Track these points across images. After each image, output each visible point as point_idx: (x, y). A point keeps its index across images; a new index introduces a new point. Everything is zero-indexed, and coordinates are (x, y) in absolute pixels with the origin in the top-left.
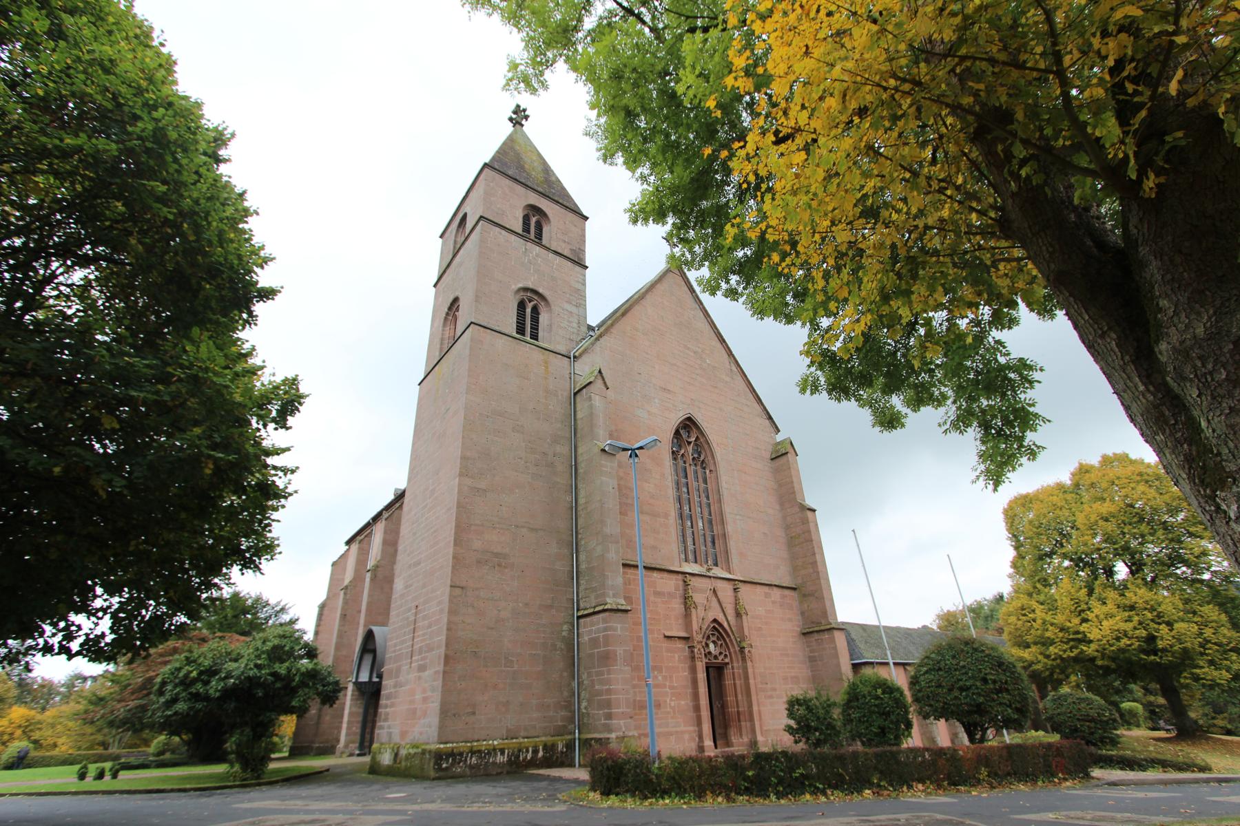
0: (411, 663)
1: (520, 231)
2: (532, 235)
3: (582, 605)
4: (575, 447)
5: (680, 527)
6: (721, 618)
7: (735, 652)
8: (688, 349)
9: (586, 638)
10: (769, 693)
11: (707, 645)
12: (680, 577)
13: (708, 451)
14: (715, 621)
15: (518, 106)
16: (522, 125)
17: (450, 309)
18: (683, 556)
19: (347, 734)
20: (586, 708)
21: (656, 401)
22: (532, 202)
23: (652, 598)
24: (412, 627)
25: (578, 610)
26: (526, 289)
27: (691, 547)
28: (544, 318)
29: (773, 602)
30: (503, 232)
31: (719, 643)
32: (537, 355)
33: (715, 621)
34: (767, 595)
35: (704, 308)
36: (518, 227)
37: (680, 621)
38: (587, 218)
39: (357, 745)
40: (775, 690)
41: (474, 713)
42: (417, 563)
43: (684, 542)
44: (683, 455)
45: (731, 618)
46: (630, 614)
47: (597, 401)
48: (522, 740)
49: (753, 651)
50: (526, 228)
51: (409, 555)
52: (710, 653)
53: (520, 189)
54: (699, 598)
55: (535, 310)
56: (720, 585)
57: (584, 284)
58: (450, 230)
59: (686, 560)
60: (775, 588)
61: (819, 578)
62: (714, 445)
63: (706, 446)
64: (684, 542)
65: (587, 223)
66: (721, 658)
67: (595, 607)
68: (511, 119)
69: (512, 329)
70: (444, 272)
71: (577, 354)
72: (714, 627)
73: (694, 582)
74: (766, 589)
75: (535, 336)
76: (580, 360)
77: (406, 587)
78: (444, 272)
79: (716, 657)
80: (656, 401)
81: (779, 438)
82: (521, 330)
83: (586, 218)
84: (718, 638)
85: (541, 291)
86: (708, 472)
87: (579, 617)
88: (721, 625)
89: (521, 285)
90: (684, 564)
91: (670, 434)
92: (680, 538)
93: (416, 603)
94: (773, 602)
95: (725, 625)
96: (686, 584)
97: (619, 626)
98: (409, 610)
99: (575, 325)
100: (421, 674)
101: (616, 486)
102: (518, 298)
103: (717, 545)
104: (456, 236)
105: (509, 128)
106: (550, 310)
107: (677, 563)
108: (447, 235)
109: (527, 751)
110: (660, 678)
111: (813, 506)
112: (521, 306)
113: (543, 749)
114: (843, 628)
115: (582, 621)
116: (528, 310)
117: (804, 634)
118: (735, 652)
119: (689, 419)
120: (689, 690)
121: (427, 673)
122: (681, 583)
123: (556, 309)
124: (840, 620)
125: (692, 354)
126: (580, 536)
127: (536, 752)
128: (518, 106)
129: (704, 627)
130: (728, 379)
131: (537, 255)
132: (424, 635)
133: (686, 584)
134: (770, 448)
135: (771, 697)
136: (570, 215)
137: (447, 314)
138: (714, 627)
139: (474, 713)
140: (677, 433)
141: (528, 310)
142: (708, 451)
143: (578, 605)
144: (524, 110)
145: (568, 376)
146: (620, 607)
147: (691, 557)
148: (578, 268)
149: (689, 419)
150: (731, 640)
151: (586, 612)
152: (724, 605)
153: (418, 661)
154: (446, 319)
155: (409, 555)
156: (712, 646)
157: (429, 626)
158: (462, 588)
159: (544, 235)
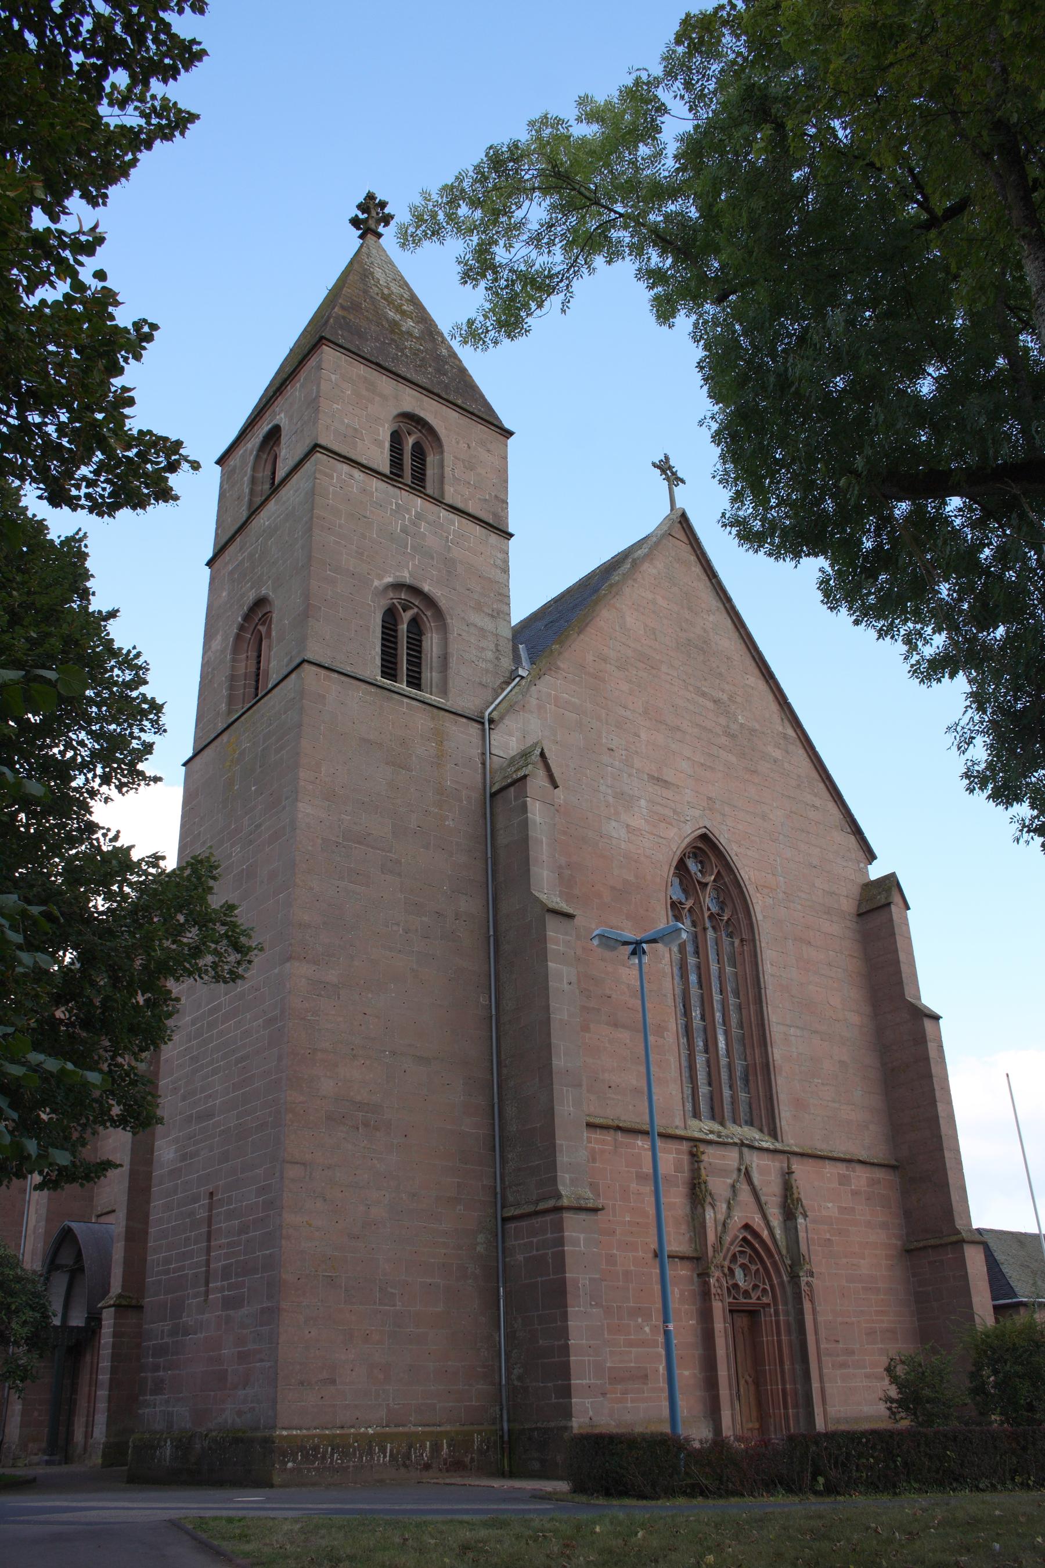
0: (207, 1293)
1: (387, 471)
2: (408, 478)
3: (511, 1199)
4: (495, 900)
5: (684, 1052)
6: (757, 1222)
7: (782, 1284)
8: (704, 695)
9: (520, 1258)
10: (841, 1359)
11: (731, 1271)
12: (685, 1146)
13: (738, 902)
14: (747, 1227)
15: (370, 197)
16: (379, 235)
17: (247, 618)
18: (689, 1106)
19: (23, 1425)
20: (520, 1378)
21: (643, 803)
22: (407, 408)
23: (634, 1186)
24: (205, 1230)
25: (503, 1207)
26: (398, 586)
27: (703, 1090)
28: (431, 643)
29: (855, 1193)
30: (357, 473)
31: (753, 1268)
32: (421, 721)
33: (747, 1227)
34: (844, 1180)
35: (733, 608)
36: (382, 460)
37: (684, 1228)
38: (509, 434)
39: (44, 1445)
40: (851, 1352)
41: (333, 1382)
42: (208, 1115)
43: (693, 1079)
44: (691, 910)
45: (776, 1222)
46: (600, 1216)
47: (537, 813)
48: (413, 1429)
49: (815, 1281)
50: (396, 461)
51: (184, 1099)
52: (736, 1286)
53: (385, 384)
54: (718, 1186)
55: (416, 627)
56: (755, 1161)
57: (506, 570)
58: (240, 451)
59: (696, 1114)
60: (859, 1168)
61: (941, 1149)
62: (751, 889)
63: (734, 892)
64: (693, 1079)
65: (511, 441)
66: (754, 1295)
67: (537, 1202)
68: (355, 222)
69: (373, 670)
70: (232, 539)
71: (495, 715)
72: (744, 1239)
73: (711, 1156)
74: (841, 1168)
75: (415, 681)
76: (501, 727)
77: (184, 1158)
78: (232, 539)
79: (746, 1294)
80: (643, 803)
81: (876, 871)
82: (389, 669)
83: (509, 434)
84: (751, 1260)
85: (426, 588)
86: (737, 942)
87: (505, 1220)
88: (756, 1235)
89: (389, 580)
90: (694, 1123)
91: (666, 870)
92: (686, 1074)
93: (210, 1188)
94: (855, 1193)
95: (765, 1234)
96: (695, 1157)
97: (582, 1236)
98: (195, 1199)
99: (489, 655)
100: (231, 1312)
101: (574, 979)
102: (384, 603)
103: (752, 1084)
104: (254, 469)
105: (352, 238)
106: (444, 628)
107: (678, 1121)
108: (233, 461)
109: (423, 1446)
110: (647, 1329)
111: (936, 1009)
112: (390, 618)
113: (449, 1446)
114: (984, 1239)
115: (512, 1225)
116: (403, 627)
117: (908, 1251)
118: (782, 1284)
119: (704, 838)
120: (698, 1352)
121: (244, 1311)
122: (685, 1158)
123: (455, 625)
124: (976, 1224)
125: (710, 705)
126: (505, 1071)
127: (436, 1448)
128: (370, 197)
129: (728, 1239)
130: (777, 754)
131: (419, 516)
132: (230, 1245)
133: (695, 1157)
134: (855, 891)
135: (844, 1365)
136: (480, 431)
137: (242, 628)
138: (744, 1239)
139: (333, 1382)
140: (681, 866)
141: (403, 627)
142: (738, 902)
143: (504, 1197)
144: (383, 205)
145: (478, 761)
146: (583, 1203)
147: (704, 1107)
148: (494, 539)
149: (704, 838)
150: (775, 1264)
151: (517, 1212)
152: (763, 1199)
153: (222, 1289)
154: (238, 638)
155: (184, 1099)
156: (739, 1273)
157: (243, 1229)
158: (304, 1164)
159: (784, 1087)
